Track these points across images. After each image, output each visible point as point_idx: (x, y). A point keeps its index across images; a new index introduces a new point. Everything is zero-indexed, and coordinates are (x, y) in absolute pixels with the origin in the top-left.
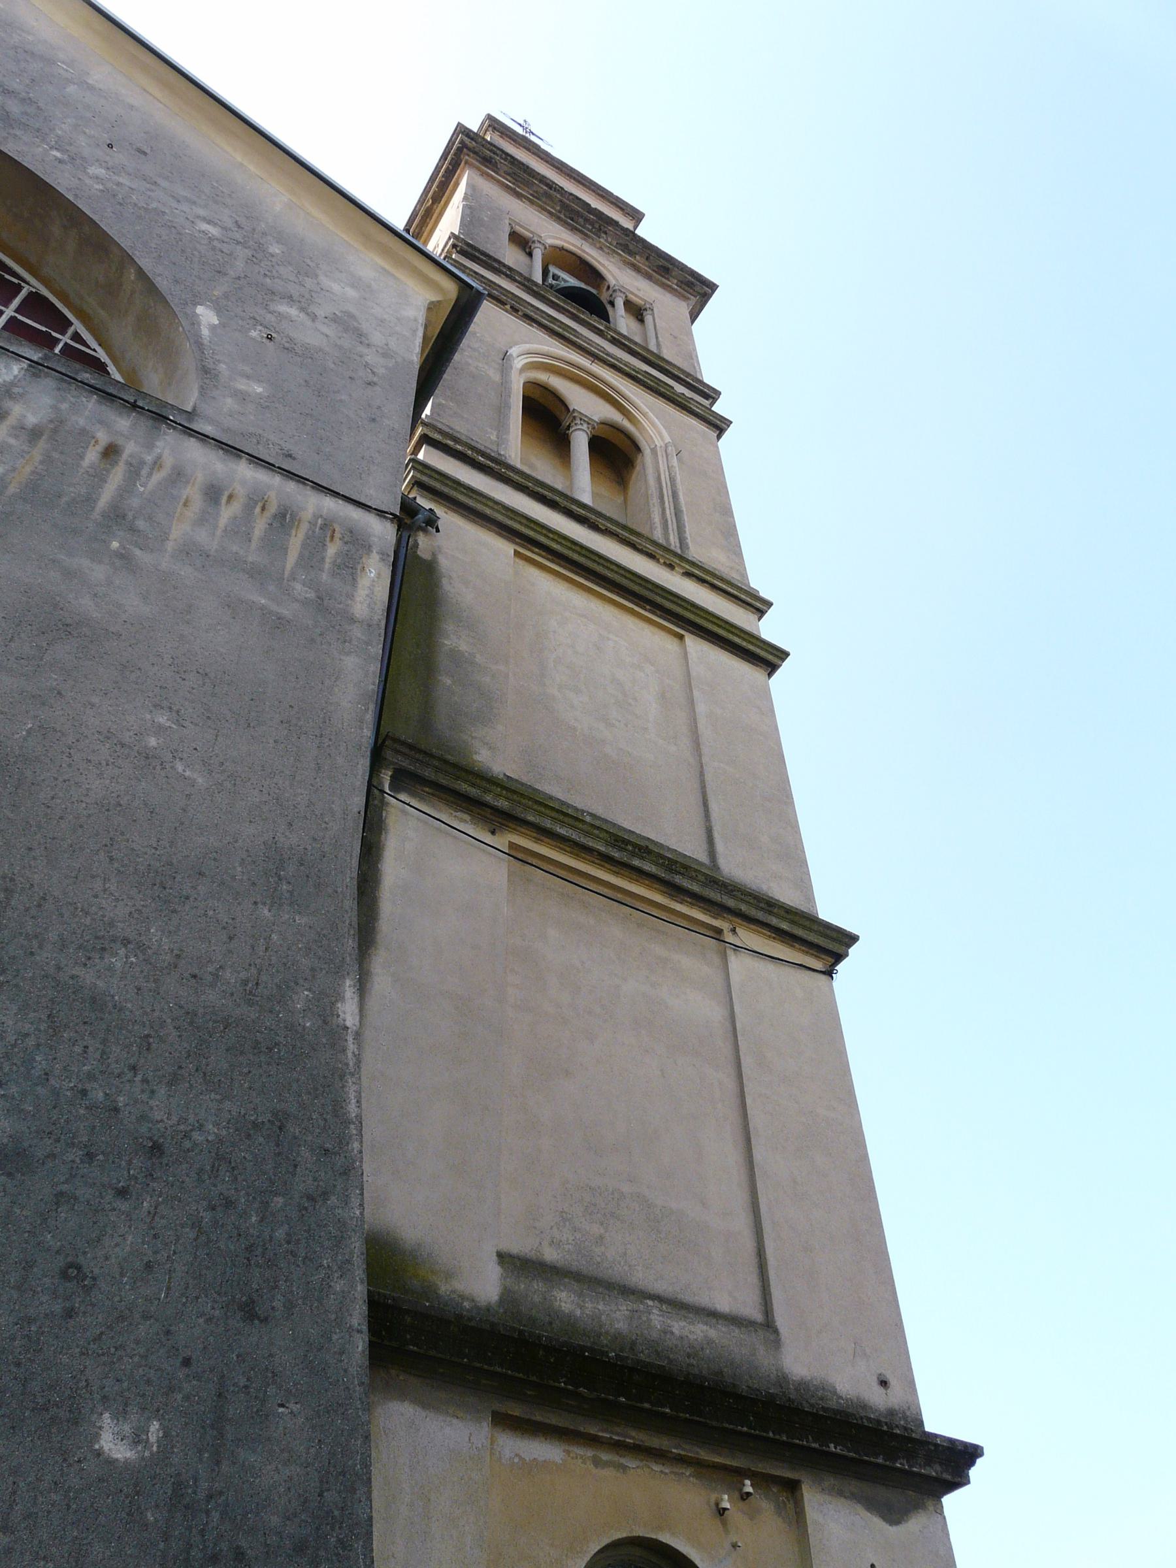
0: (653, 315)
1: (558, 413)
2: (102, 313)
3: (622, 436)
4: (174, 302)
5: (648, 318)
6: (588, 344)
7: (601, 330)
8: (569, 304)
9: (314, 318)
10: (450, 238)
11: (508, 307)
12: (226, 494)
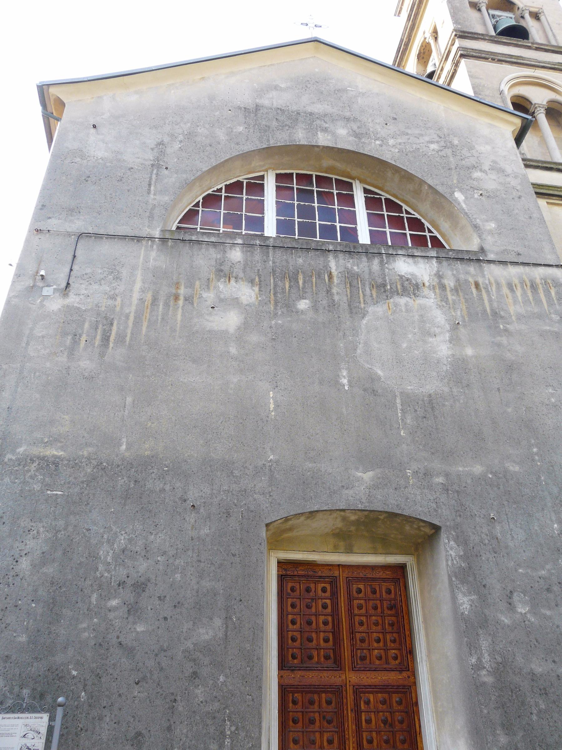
0: (544, 15)
1: (526, 106)
2: (414, 201)
3: (557, 104)
4: (447, 196)
5: (542, 18)
6: (529, 61)
7: (530, 46)
8: (513, 39)
9: (484, 172)
10: (453, 32)
11: (490, 60)
12: (514, 285)
